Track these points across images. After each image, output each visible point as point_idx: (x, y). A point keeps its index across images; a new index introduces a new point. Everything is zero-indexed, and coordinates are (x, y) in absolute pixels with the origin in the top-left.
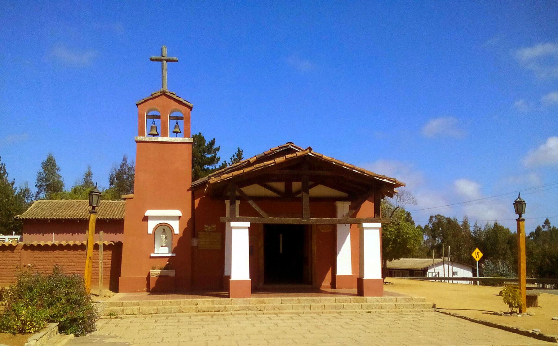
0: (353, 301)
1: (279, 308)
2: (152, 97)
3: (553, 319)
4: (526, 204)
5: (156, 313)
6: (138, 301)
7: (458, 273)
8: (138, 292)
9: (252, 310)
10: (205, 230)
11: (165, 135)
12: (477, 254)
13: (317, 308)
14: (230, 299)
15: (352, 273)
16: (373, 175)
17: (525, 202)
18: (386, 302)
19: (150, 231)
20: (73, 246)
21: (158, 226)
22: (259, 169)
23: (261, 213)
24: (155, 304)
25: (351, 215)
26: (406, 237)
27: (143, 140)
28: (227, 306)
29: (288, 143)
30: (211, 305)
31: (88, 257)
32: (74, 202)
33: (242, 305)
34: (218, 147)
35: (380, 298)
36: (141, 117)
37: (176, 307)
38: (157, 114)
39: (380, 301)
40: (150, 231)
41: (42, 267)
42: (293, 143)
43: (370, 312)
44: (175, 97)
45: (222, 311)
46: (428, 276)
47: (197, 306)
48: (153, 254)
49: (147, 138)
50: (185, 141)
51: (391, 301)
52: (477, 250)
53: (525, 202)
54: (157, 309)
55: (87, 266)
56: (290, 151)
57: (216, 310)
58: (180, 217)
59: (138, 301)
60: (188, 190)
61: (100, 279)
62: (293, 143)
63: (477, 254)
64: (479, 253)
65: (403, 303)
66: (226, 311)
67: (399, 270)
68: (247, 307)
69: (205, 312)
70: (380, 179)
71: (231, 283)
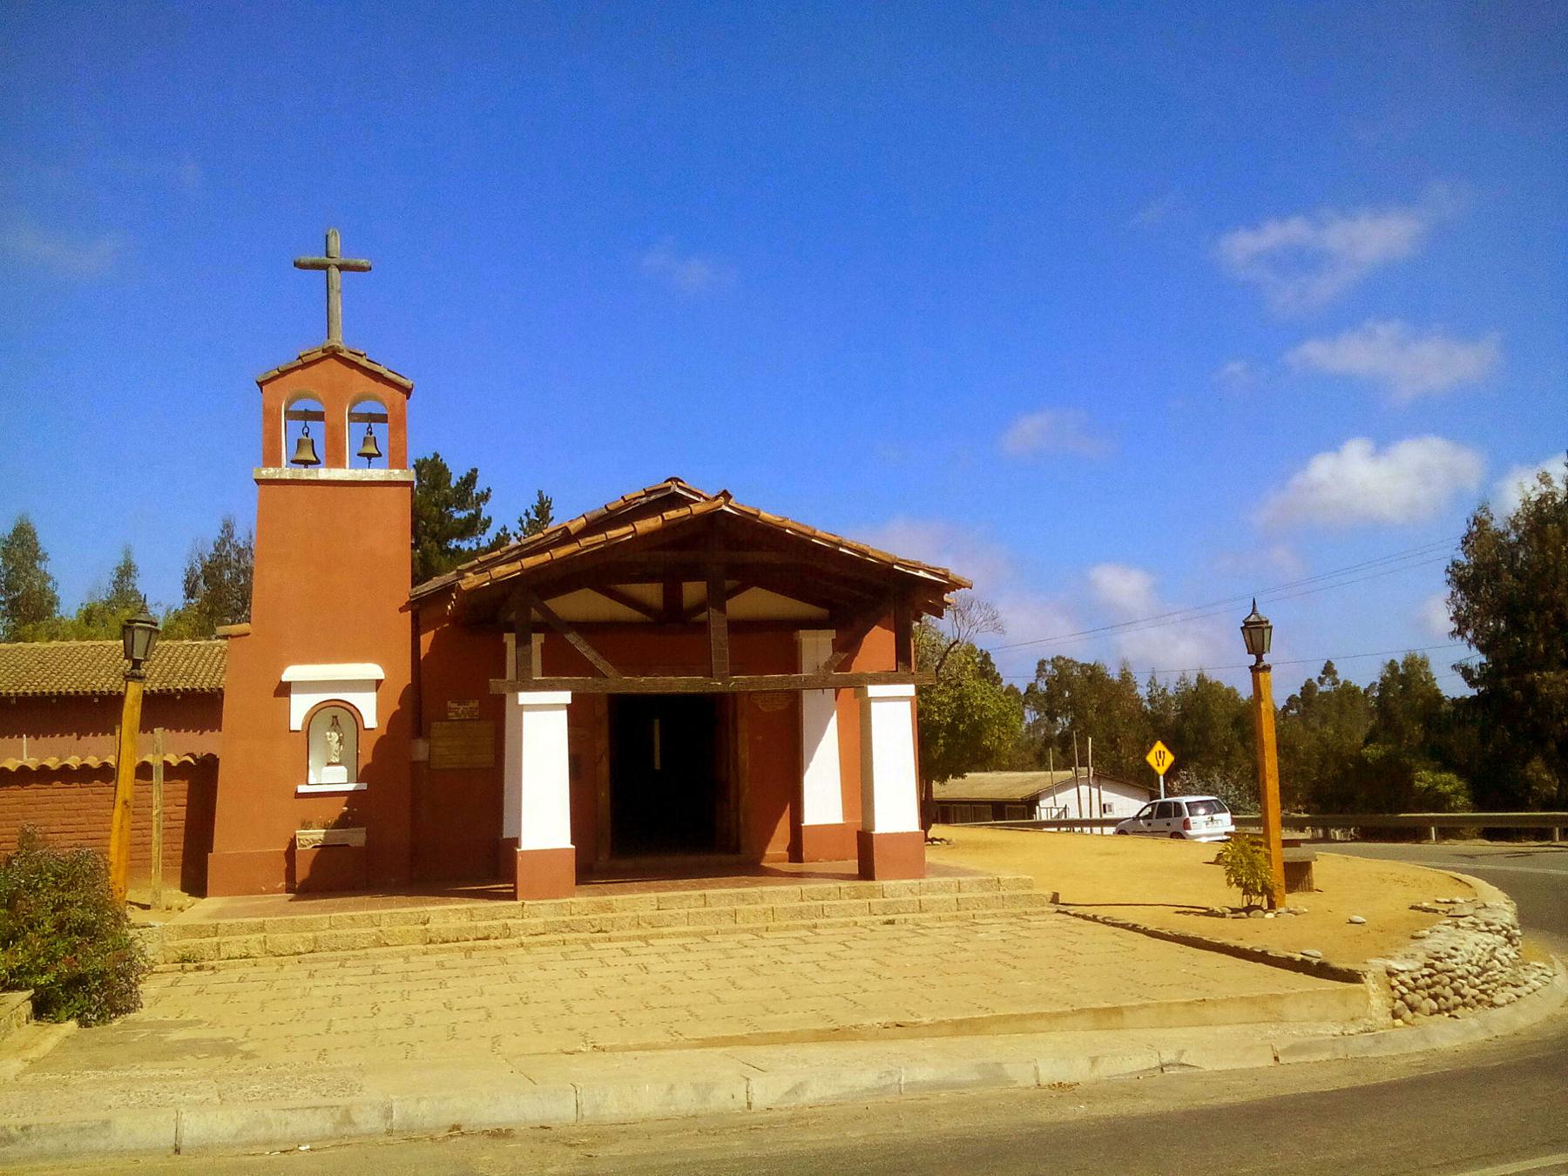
1: (650, 924)
2: (300, 362)
3: (1351, 922)
4: (1271, 627)
5: (312, 952)
6: (261, 920)
7: (1115, 808)
8: (262, 893)
10: (450, 714)
11: (338, 462)
12: (1160, 757)
14: (519, 902)
17: (1270, 624)
18: (934, 892)
19: (296, 723)
20: (77, 770)
21: (320, 706)
22: (595, 548)
23: (602, 665)
24: (309, 926)
25: (836, 665)
26: (980, 717)
27: (277, 477)
28: (510, 922)
29: (670, 480)
30: (465, 922)
32: (83, 647)
33: (550, 919)
35: (916, 882)
36: (270, 416)
37: (364, 931)
38: (313, 406)
40: (296, 723)
42: (682, 481)
44: (363, 362)
45: (496, 938)
46: (1040, 818)
48: (306, 786)
49: (287, 472)
50: (393, 479)
51: (945, 889)
52: (1159, 746)
53: (1270, 624)
54: (316, 940)
55: (116, 826)
56: (674, 501)
57: (480, 936)
58: (379, 682)
59: (261, 920)
61: (154, 861)
62: (682, 481)
63: (1160, 757)
64: (1164, 752)
65: (977, 894)
66: (508, 937)
69: (447, 942)
70: (908, 571)
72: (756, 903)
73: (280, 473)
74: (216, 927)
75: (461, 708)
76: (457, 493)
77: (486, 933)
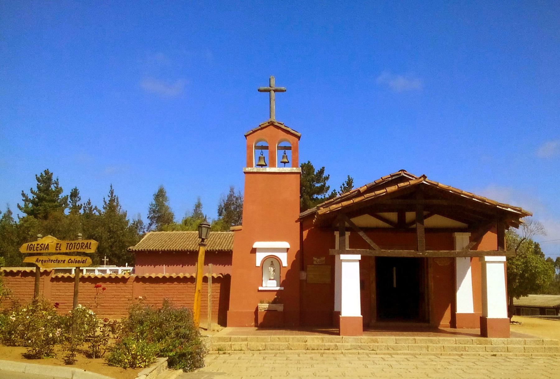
0: (476, 343)
1: (393, 349)
5: (264, 350)
8: (246, 326)
9: (364, 350)
11: (273, 165)
13: (435, 350)
14: (341, 337)
15: (474, 311)
16: (495, 204)
18: (514, 344)
19: (258, 264)
23: (373, 245)
24: (263, 340)
26: (535, 271)
27: (252, 171)
28: (337, 344)
29: (401, 171)
30: (320, 343)
31: (197, 290)
32: (184, 233)
34: (327, 176)
35: (506, 339)
36: (249, 148)
38: (265, 144)
39: (505, 343)
40: (258, 264)
41: (153, 299)
43: (495, 355)
44: (283, 127)
47: (306, 343)
49: (255, 169)
50: (293, 171)
54: (266, 345)
56: (402, 179)
58: (288, 249)
59: (246, 336)
60: (296, 222)
61: (209, 312)
67: (536, 307)
68: (358, 345)
69: (314, 350)
71: (341, 319)
72: (437, 344)
73: (253, 170)
74: (230, 338)
75: (318, 260)
76: (317, 176)
77: (328, 348)
